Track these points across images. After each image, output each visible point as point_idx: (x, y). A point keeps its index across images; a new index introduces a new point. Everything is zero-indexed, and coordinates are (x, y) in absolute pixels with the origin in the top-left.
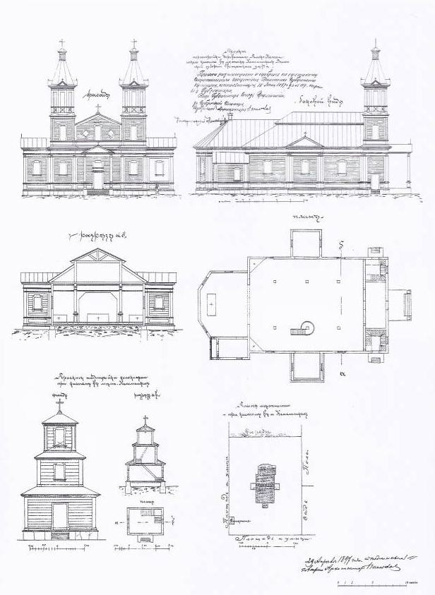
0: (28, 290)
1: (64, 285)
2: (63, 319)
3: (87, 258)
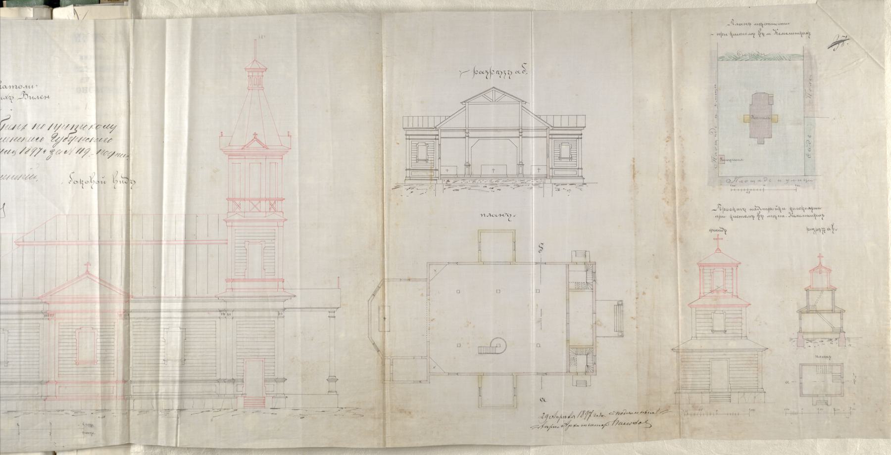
0: (411, 137)
1: (453, 130)
2: (452, 172)
3: (481, 99)
